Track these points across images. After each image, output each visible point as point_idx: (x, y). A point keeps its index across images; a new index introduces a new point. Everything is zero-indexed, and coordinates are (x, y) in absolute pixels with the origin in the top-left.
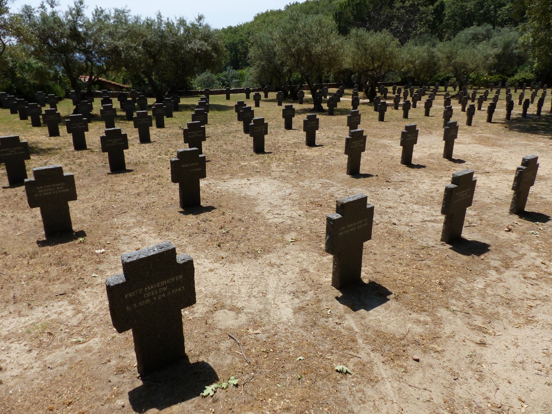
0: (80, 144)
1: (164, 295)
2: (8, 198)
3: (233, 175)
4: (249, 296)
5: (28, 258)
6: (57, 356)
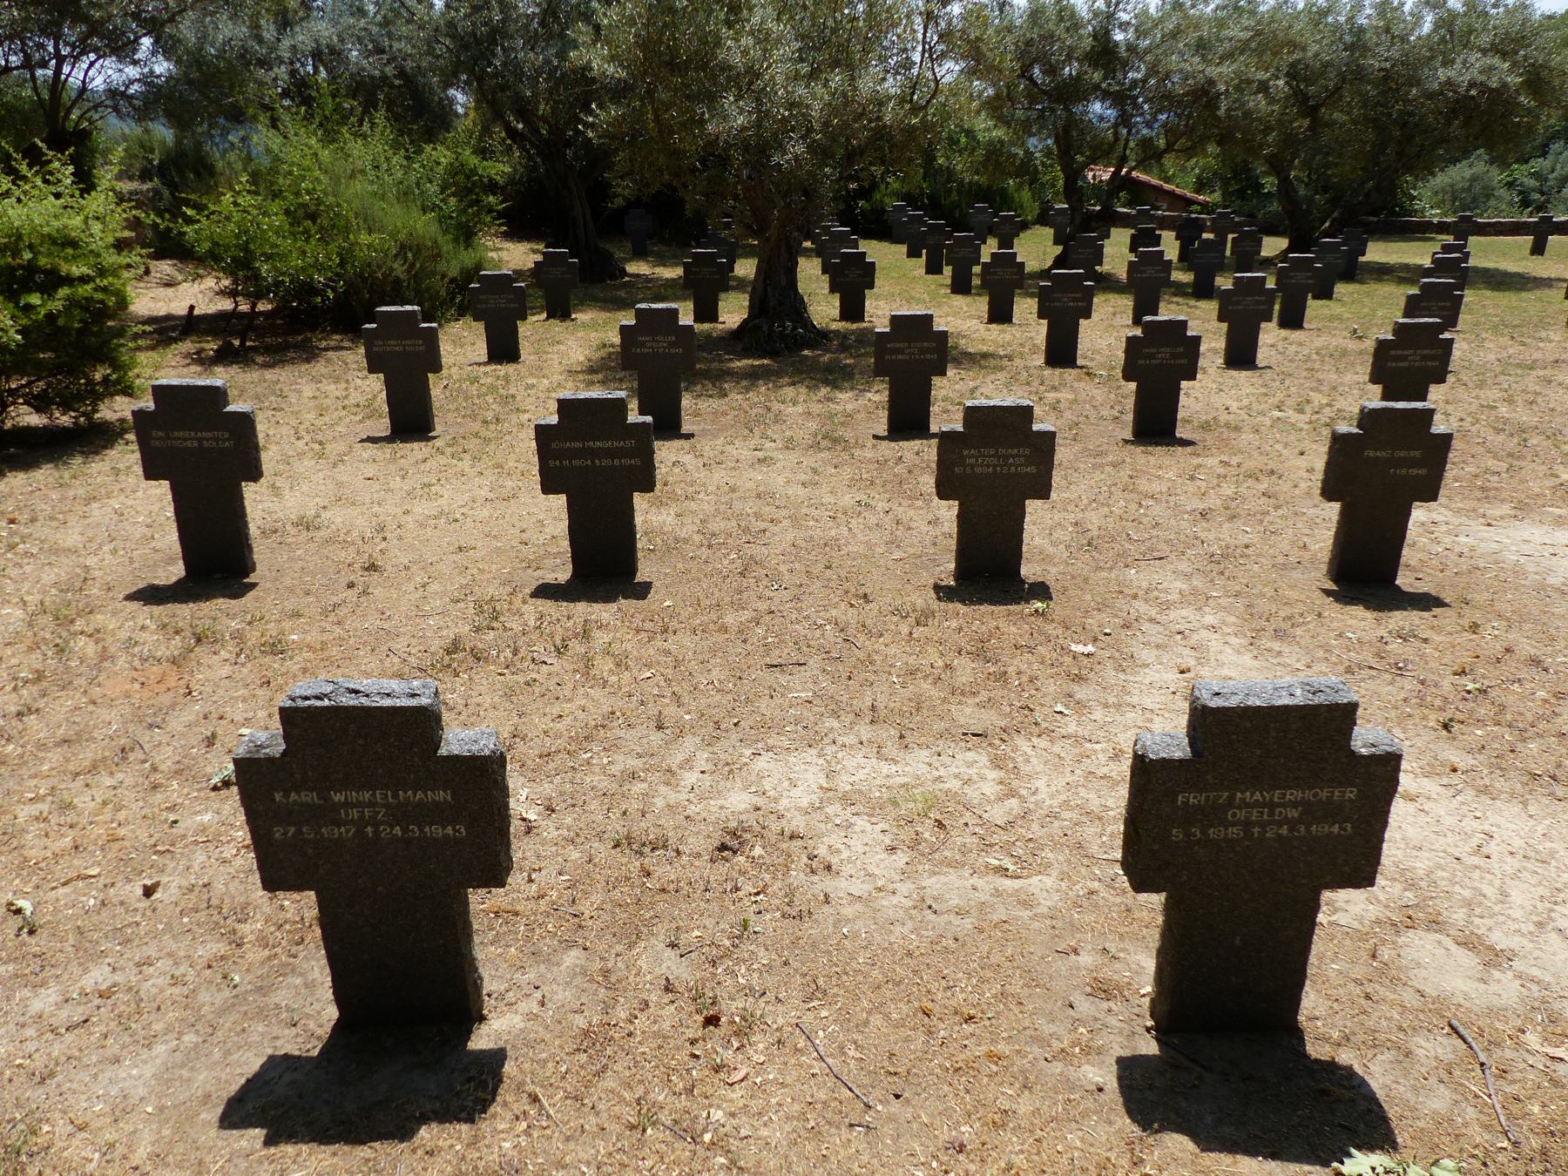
0: (1061, 352)
1: (1284, 831)
2: (881, 464)
3: (1523, 509)
4: (1540, 925)
5: (911, 620)
6: (952, 886)
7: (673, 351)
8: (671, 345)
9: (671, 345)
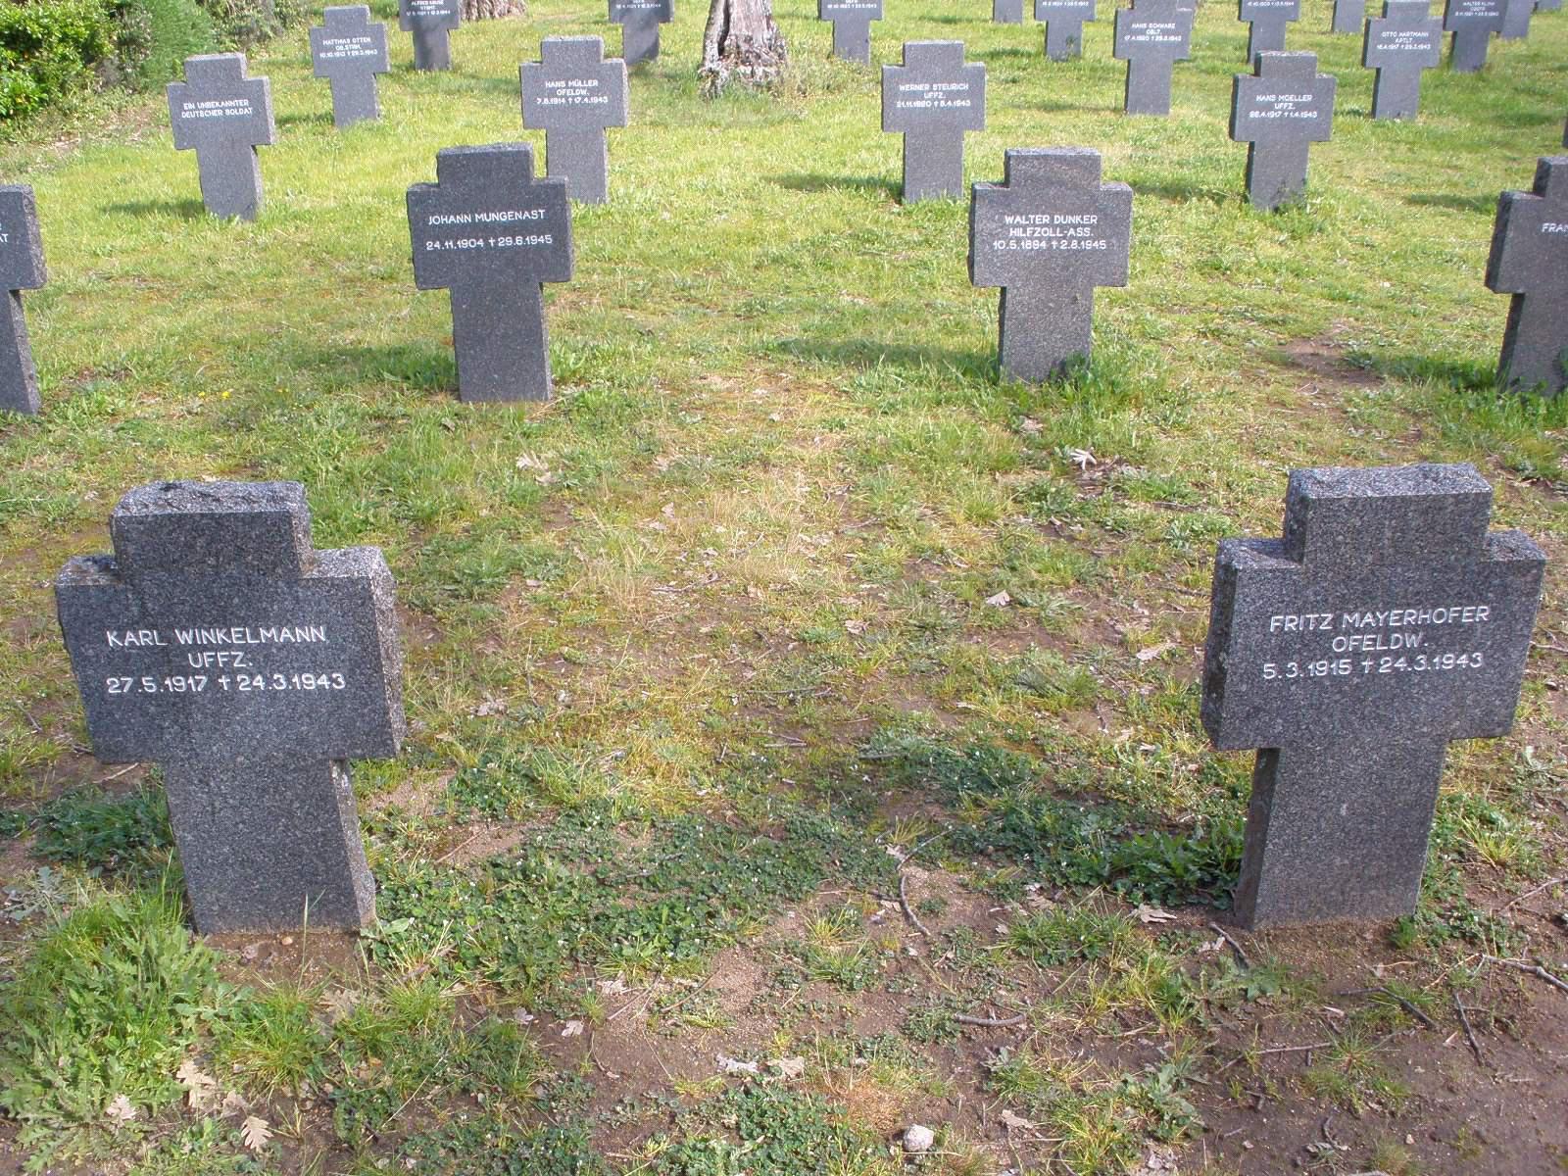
1: (1401, 664)
7: (595, 100)
8: (592, 92)
9: (592, 92)
